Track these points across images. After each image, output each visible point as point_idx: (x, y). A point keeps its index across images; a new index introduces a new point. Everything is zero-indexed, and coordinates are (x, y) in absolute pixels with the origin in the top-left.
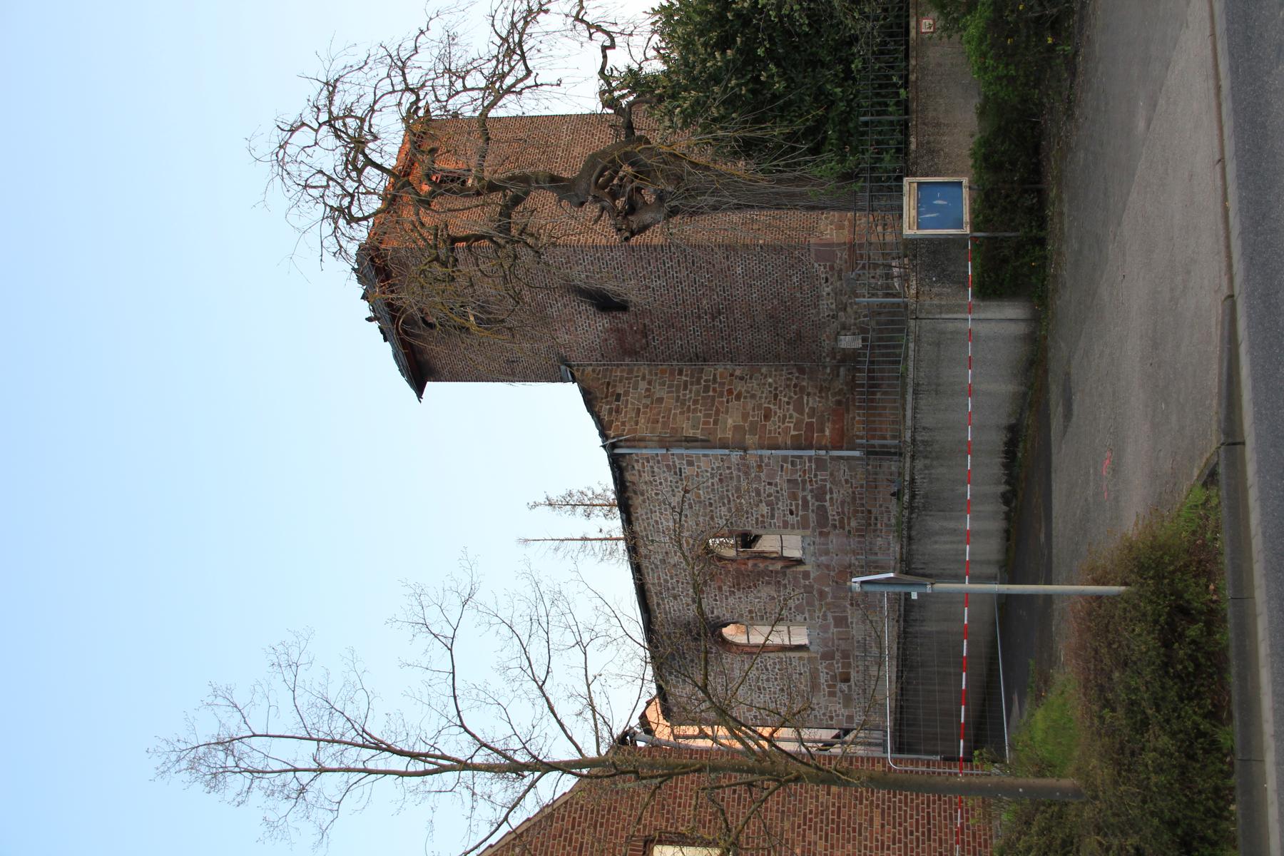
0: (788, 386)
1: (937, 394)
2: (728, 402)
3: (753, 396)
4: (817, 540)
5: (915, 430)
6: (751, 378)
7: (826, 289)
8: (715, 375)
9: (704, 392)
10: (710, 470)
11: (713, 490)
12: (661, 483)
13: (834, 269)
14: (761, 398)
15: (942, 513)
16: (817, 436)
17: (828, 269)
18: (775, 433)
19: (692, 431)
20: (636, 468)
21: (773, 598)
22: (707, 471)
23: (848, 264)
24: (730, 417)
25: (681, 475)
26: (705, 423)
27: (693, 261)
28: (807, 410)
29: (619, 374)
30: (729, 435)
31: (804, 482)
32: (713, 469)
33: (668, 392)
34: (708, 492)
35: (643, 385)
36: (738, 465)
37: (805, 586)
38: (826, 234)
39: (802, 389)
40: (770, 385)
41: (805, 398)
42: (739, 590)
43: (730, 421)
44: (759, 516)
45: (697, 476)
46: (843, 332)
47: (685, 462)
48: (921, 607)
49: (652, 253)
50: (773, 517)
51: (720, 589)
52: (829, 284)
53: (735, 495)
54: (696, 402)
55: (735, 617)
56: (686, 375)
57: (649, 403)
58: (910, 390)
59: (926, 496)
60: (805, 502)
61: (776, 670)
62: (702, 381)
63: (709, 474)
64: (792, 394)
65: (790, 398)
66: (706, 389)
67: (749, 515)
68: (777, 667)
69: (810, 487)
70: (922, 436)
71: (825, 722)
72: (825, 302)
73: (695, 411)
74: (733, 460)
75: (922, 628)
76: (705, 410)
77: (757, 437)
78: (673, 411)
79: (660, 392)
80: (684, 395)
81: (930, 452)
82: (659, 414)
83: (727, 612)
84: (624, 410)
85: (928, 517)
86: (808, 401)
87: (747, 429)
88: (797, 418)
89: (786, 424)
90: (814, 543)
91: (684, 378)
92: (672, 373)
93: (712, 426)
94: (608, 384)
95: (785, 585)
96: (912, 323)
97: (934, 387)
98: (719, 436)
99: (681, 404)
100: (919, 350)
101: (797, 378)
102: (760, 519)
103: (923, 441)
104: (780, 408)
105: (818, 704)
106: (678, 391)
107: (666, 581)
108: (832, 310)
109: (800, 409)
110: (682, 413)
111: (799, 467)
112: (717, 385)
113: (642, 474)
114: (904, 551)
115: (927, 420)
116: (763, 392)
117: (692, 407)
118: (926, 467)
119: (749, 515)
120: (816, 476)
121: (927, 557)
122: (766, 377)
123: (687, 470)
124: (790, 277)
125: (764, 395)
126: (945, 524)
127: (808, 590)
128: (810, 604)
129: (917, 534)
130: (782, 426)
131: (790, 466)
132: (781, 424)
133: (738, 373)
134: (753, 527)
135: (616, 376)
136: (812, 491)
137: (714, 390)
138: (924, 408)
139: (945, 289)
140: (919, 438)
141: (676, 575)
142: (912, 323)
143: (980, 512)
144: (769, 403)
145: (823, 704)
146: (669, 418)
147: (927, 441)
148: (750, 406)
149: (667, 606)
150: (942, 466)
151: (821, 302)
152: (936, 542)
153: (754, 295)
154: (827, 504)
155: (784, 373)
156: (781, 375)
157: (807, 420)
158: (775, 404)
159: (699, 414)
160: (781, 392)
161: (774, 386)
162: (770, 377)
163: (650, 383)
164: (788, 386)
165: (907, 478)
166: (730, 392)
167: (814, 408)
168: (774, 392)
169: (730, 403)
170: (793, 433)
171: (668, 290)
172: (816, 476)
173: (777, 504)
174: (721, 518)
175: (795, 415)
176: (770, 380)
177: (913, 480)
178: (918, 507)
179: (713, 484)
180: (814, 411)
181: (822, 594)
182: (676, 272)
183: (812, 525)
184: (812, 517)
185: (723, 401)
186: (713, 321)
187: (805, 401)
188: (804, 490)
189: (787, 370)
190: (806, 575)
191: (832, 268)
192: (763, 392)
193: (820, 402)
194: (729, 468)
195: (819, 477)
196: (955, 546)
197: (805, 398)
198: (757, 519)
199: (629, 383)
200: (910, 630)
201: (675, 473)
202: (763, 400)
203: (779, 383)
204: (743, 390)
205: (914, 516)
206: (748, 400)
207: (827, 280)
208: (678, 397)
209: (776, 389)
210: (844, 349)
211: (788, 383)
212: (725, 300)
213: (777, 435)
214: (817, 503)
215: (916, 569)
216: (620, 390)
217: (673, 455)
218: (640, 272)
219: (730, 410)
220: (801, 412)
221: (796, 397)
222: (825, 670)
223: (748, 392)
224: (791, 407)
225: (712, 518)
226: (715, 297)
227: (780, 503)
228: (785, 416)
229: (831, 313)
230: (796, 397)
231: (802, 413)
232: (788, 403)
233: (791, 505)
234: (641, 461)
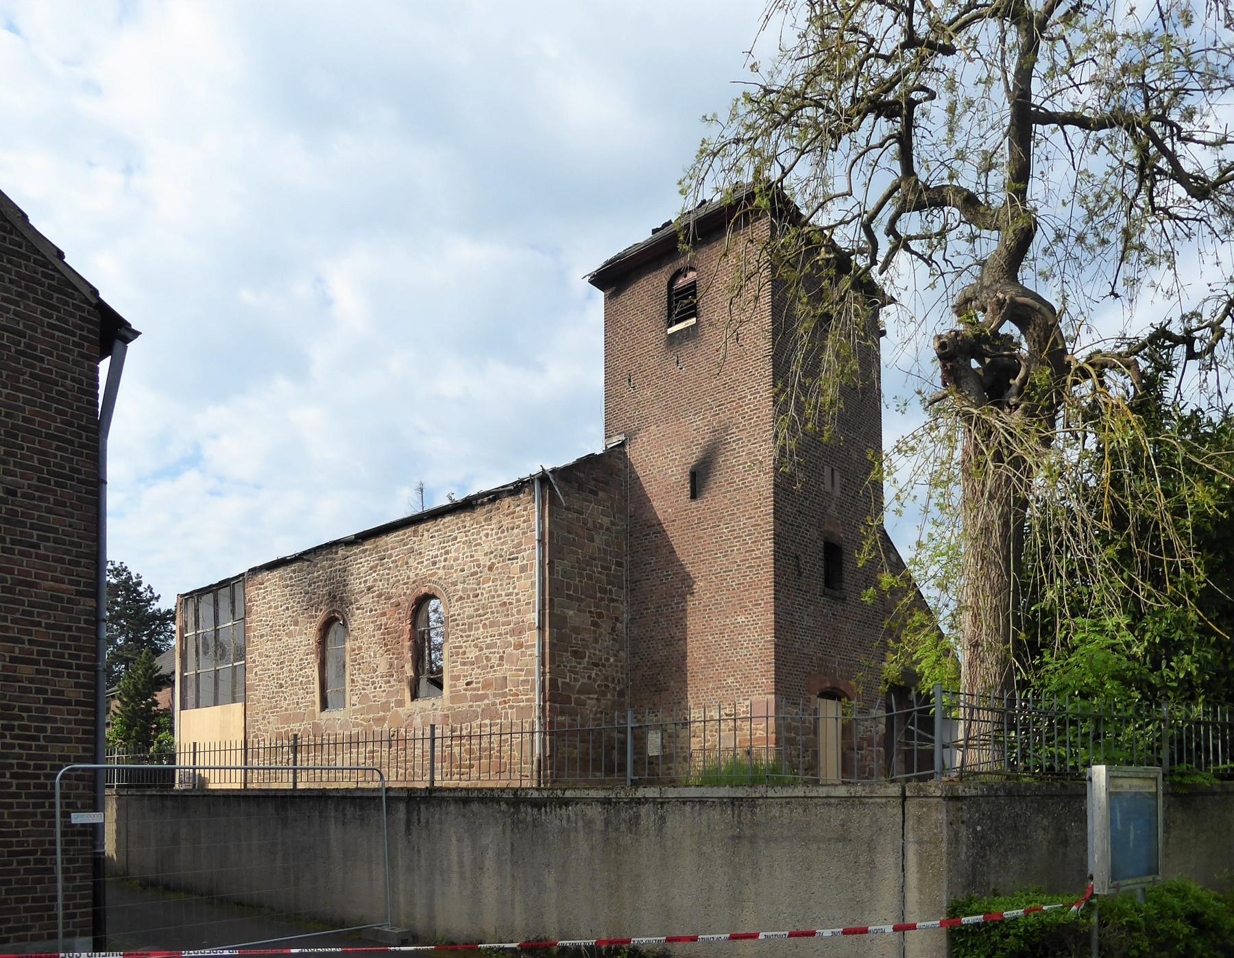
0: (606, 679)
1: (733, 837)
2: (590, 612)
3: (596, 641)
4: (439, 713)
5: (662, 803)
8: (617, 601)
10: (516, 591)
11: (493, 597)
12: (499, 539)
15: (508, 849)
20: (517, 509)
21: (375, 671)
22: (514, 588)
24: (575, 614)
25: (509, 559)
26: (569, 585)
27: (753, 567)
31: (504, 695)
32: (517, 594)
34: (490, 591)
35: (606, 521)
36: (523, 621)
37: (388, 703)
39: (604, 694)
40: (607, 660)
41: (595, 696)
42: (382, 634)
43: (571, 613)
44: (464, 649)
45: (509, 578)
46: (666, 735)
47: (525, 562)
48: (362, 820)
49: (762, 520)
50: (464, 664)
51: (384, 614)
53: (487, 622)
54: (590, 577)
55: (354, 633)
56: (616, 570)
58: (740, 793)
59: (536, 824)
60: (482, 698)
61: (301, 679)
63: (511, 590)
64: (599, 682)
67: (465, 639)
68: (304, 680)
69: (498, 701)
70: (648, 815)
71: (252, 730)
73: (581, 575)
74: (528, 615)
75: (333, 821)
79: (600, 539)
81: (617, 830)
83: (359, 624)
85: (501, 828)
86: (592, 699)
90: (436, 709)
95: (389, 682)
96: (894, 790)
97: (748, 832)
100: (830, 805)
101: (614, 689)
102: (461, 651)
103: (638, 817)
104: (584, 668)
105: (269, 723)
107: (390, 556)
109: (585, 690)
110: (578, 561)
111: (521, 688)
113: (510, 517)
114: (446, 794)
115: (676, 822)
117: (585, 573)
118: (589, 824)
119: (465, 639)
120: (512, 707)
121: (438, 826)
122: (615, 655)
123: (516, 566)
124: (733, 676)
125: (597, 652)
126: (491, 854)
127: (385, 707)
128: (370, 710)
129: (472, 812)
131: (521, 678)
133: (618, 625)
134: (452, 643)
136: (494, 704)
137: (602, 599)
138: (704, 817)
139: (964, 849)
140: (643, 810)
141: (397, 566)
142: (894, 790)
143: (513, 905)
145: (270, 727)
147: (637, 824)
148: (587, 636)
149: (363, 560)
150: (592, 849)
152: (460, 840)
157: (573, 697)
160: (601, 671)
161: (607, 664)
162: (615, 661)
163: (607, 529)
164: (606, 679)
165: (568, 794)
166: (600, 616)
167: (585, 705)
173: (478, 668)
174: (461, 609)
175: (578, 684)
176: (612, 660)
177: (566, 803)
178: (518, 811)
179: (499, 596)
181: (381, 720)
183: (455, 706)
184: (464, 706)
186: (679, 596)
187: (591, 696)
188: (495, 695)
190: (400, 703)
192: (600, 651)
193: (591, 711)
194: (519, 612)
195: (510, 711)
196: (455, 868)
197: (595, 696)
198: (461, 647)
200: (331, 806)
201: (511, 554)
202: (592, 651)
205: (504, 807)
209: (604, 666)
214: (480, 710)
215: (419, 812)
217: (534, 548)
218: (738, 509)
220: (580, 692)
222: (302, 728)
223: (600, 636)
224: (586, 680)
225: (461, 598)
227: (479, 671)
228: (576, 673)
233: (477, 683)
234: (525, 513)
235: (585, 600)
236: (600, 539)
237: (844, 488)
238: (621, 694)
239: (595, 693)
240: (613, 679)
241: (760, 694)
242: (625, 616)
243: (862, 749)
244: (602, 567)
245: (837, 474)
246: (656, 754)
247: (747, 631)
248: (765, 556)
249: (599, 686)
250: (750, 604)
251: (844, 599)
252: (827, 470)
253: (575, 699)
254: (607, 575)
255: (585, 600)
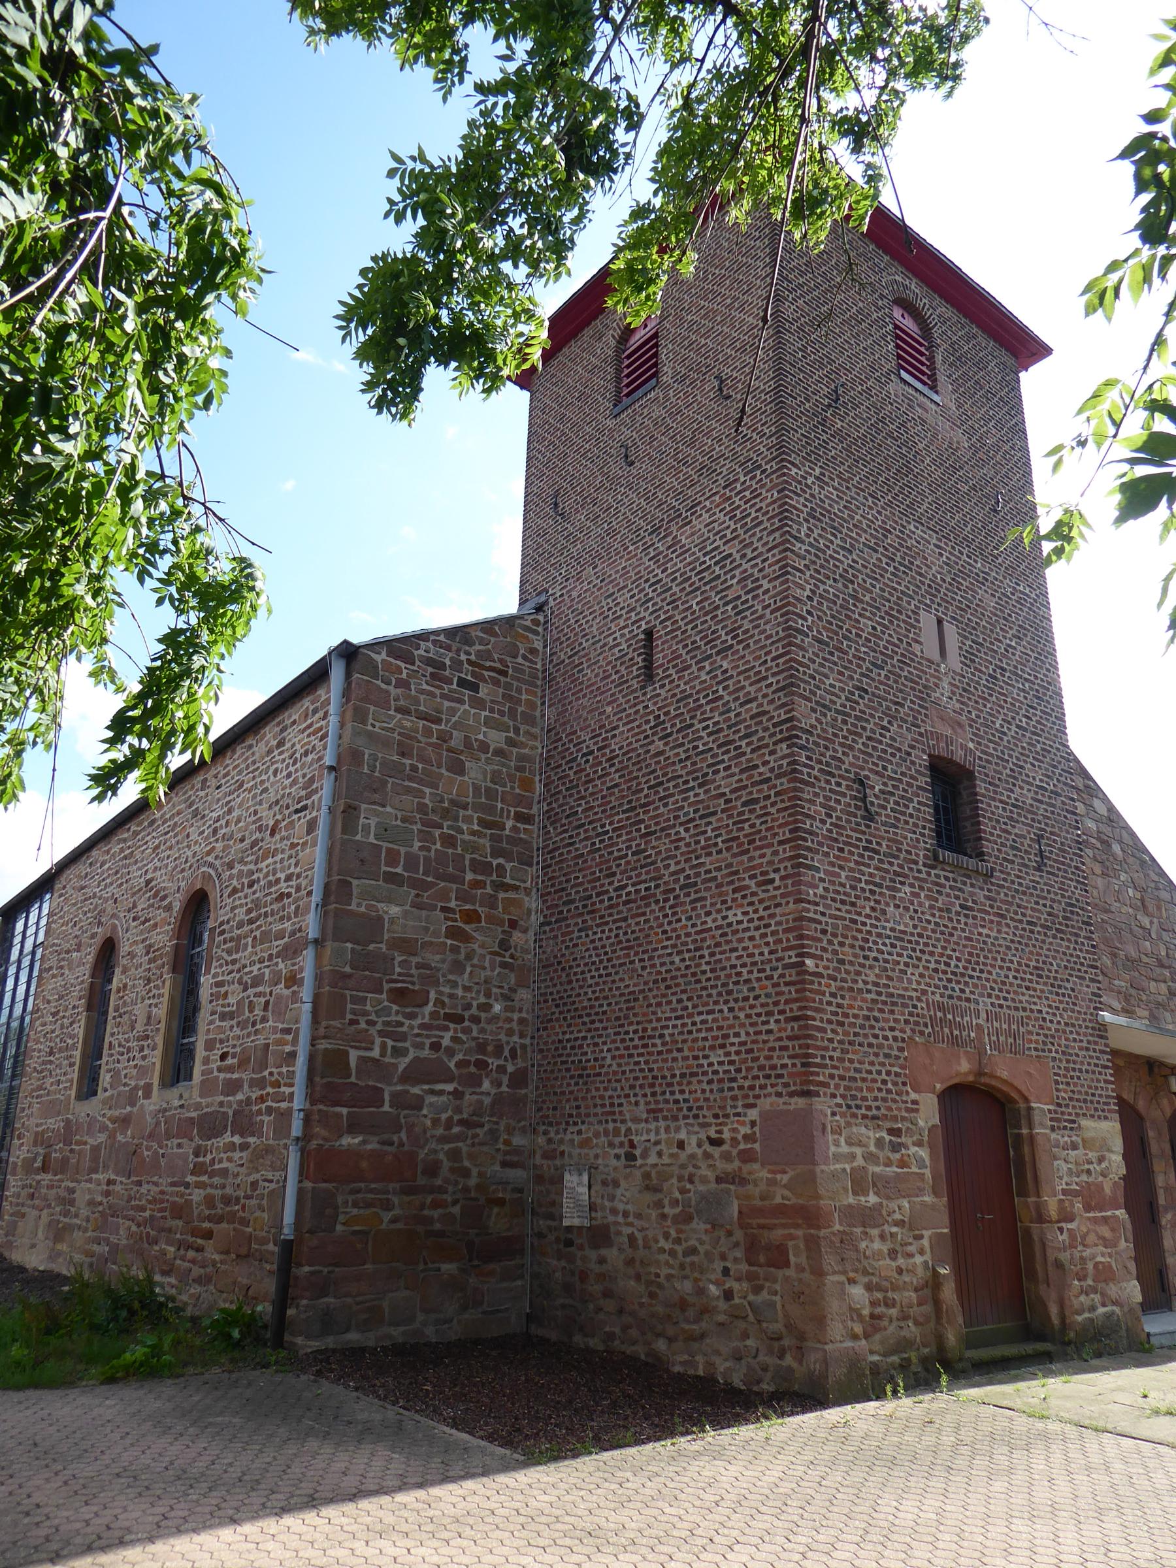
2: (444, 909)
6: (504, 965)
7: (694, 1141)
8: (516, 888)
9: (472, 860)
13: (744, 1161)
14: (454, 985)
16: (340, 1115)
17: (742, 1146)
18: (354, 1012)
19: (373, 822)
23: (757, 1203)
24: (406, 912)
27: (756, 801)
28: (416, 1090)
29: (524, 697)
30: (356, 906)
33: (476, 788)
35: (496, 738)
38: (837, 1144)
40: (486, 1007)
43: (394, 910)
52: (707, 1147)
54: (449, 841)
56: (515, 829)
57: (453, 743)
62: (501, 860)
65: (450, 1052)
66: (481, 867)
72: (663, 1136)
73: (426, 837)
76: (426, 859)
77: (348, 969)
78: (427, 791)
79: (476, 771)
80: (468, 820)
82: (422, 759)
84: (438, 692)
86: (441, 1093)
87: (371, 947)
88: (395, 1066)
89: (378, 1041)
91: (509, 824)
92: (520, 801)
93: (384, 868)
94: (504, 673)
98: (355, 882)
99: (447, 810)
101: (501, 1069)
104: (423, 1026)
106: (477, 807)
108: (645, 1155)
109: (419, 1073)
110: (422, 809)
112: (489, 890)
116: (467, 989)
120: (270, 1111)
122: (506, 998)
125: (460, 992)
130: (373, 1031)
132: (379, 1027)
133: (517, 937)
135: (519, 691)
137: (476, 884)
144: (439, 1002)
146: (410, 779)
148: (434, 959)
151: (662, 1124)
153: (677, 959)
154: (228, 1138)
155: (516, 1038)
156: (510, 1033)
158: (433, 1015)
159: (417, 844)
160: (467, 1031)
162: (507, 1009)
163: (499, 752)
164: (481, 1048)
166: (471, 917)
167: (420, 1108)
168: (467, 1014)
169: (442, 915)
170: (353, 1055)
171: (687, 758)
172: (270, 1111)
175: (404, 1062)
176: (497, 1008)
180: (413, 1108)
182: (727, 768)
185: (449, 900)
189: (523, 1047)
191: (747, 1157)
192: (467, 989)
193: (436, 1122)
197: (449, 1087)
199: (502, 713)
203: (488, 1027)
204: (476, 946)
206: (450, 957)
207: (716, 1142)
208: (465, 807)
209: (476, 1020)
210: (561, 1179)
211: (490, 1048)
212: (665, 892)
213: (349, 1016)
216: (484, 692)
219: (424, 913)
220: (409, 1077)
221: (452, 1065)
223: (469, 957)
224: (426, 1053)
226: (673, 868)
229: (638, 1152)
230: (452, 1065)
231: (406, 1078)
232: (436, 1046)
235: (434, 884)
236: (476, 771)
237: (968, 658)
238: (519, 1079)
239: (450, 1080)
240: (499, 1049)
241: (779, 1095)
242: (533, 917)
243: (1071, 1220)
244: (481, 822)
245: (950, 630)
246: (576, 1222)
247: (747, 943)
248: (778, 776)
249: (459, 1064)
250: (752, 883)
251: (989, 875)
252: (927, 621)
253: (394, 1095)
254: (493, 838)
255: (434, 884)
